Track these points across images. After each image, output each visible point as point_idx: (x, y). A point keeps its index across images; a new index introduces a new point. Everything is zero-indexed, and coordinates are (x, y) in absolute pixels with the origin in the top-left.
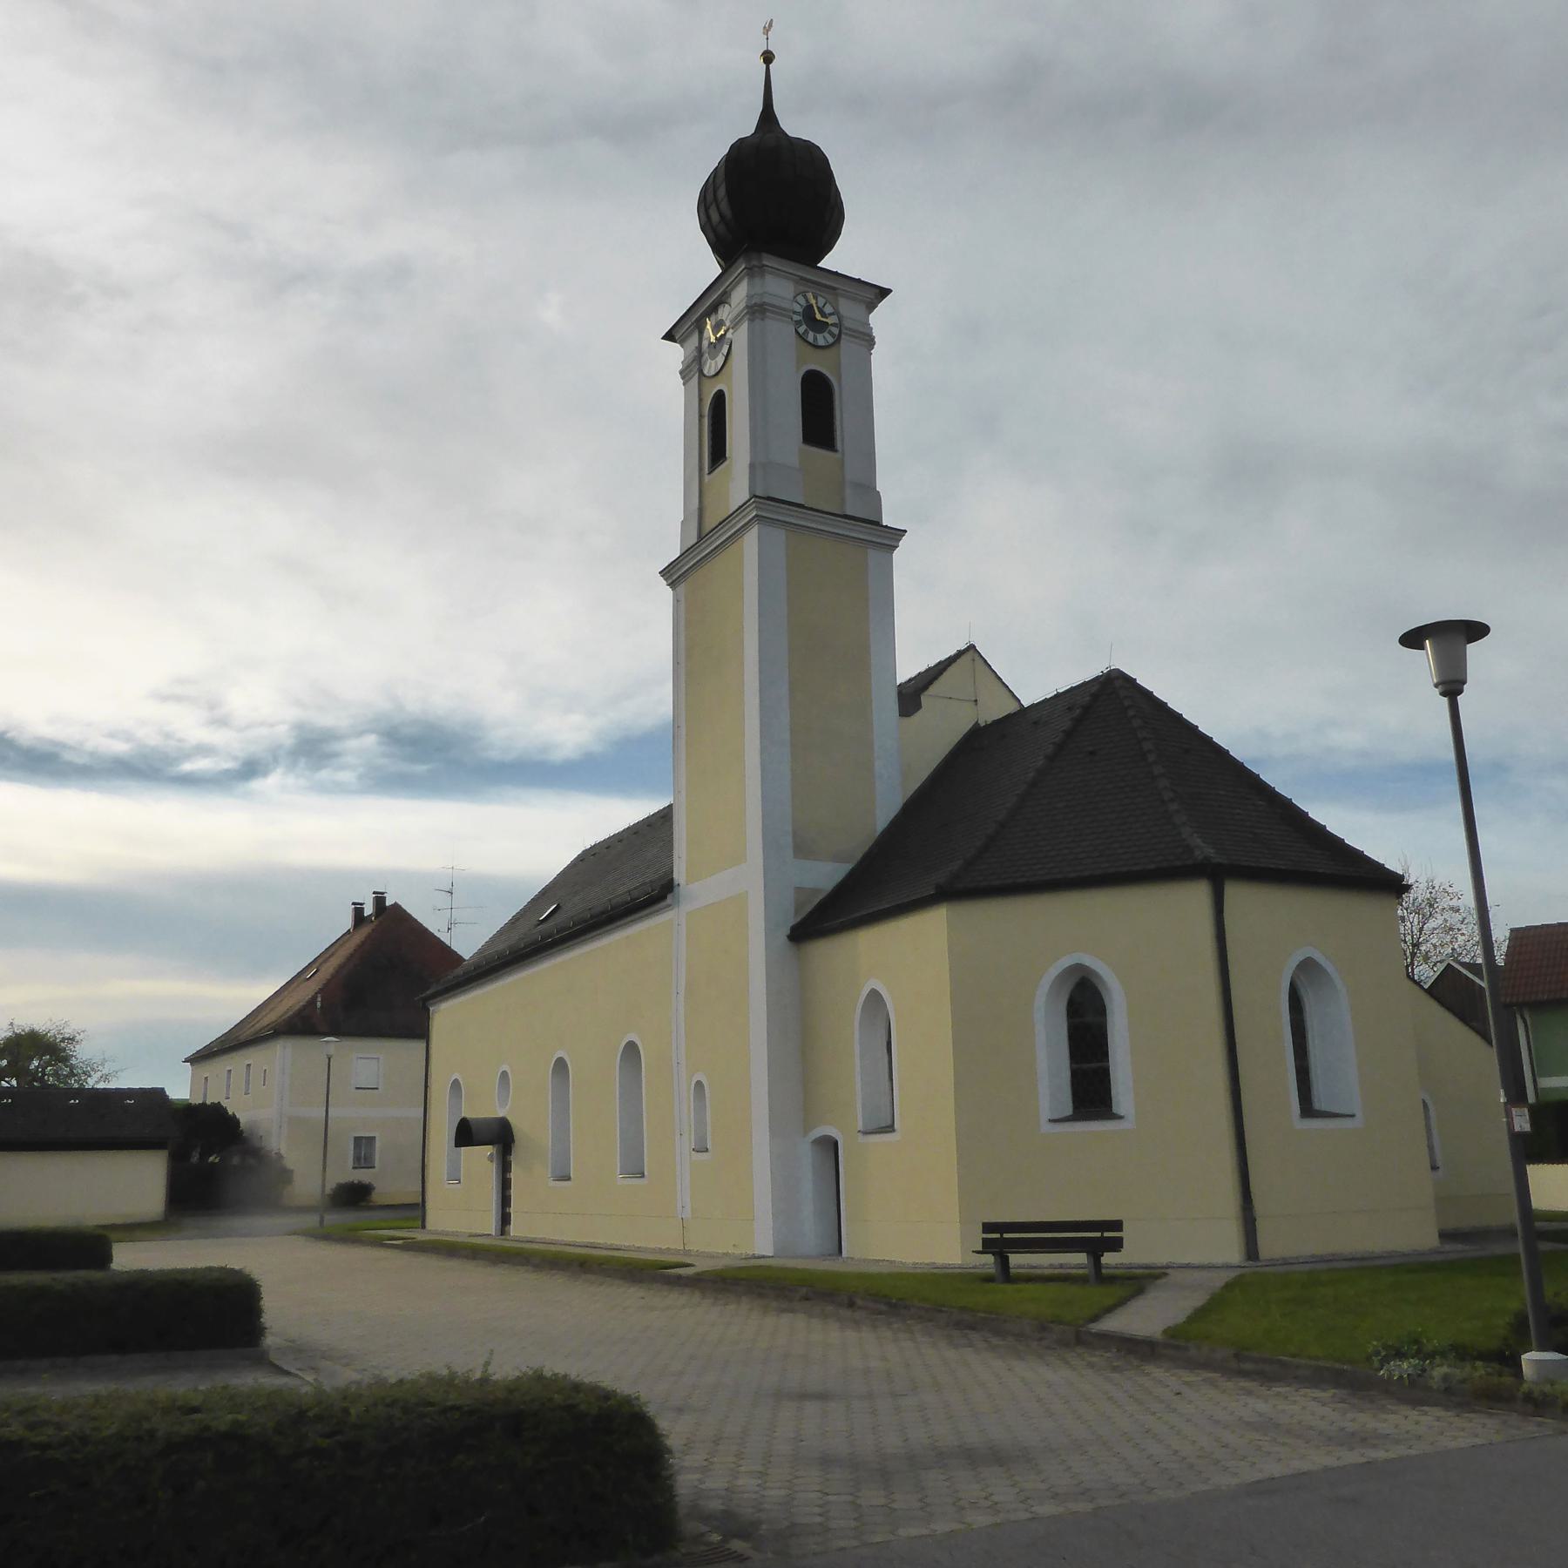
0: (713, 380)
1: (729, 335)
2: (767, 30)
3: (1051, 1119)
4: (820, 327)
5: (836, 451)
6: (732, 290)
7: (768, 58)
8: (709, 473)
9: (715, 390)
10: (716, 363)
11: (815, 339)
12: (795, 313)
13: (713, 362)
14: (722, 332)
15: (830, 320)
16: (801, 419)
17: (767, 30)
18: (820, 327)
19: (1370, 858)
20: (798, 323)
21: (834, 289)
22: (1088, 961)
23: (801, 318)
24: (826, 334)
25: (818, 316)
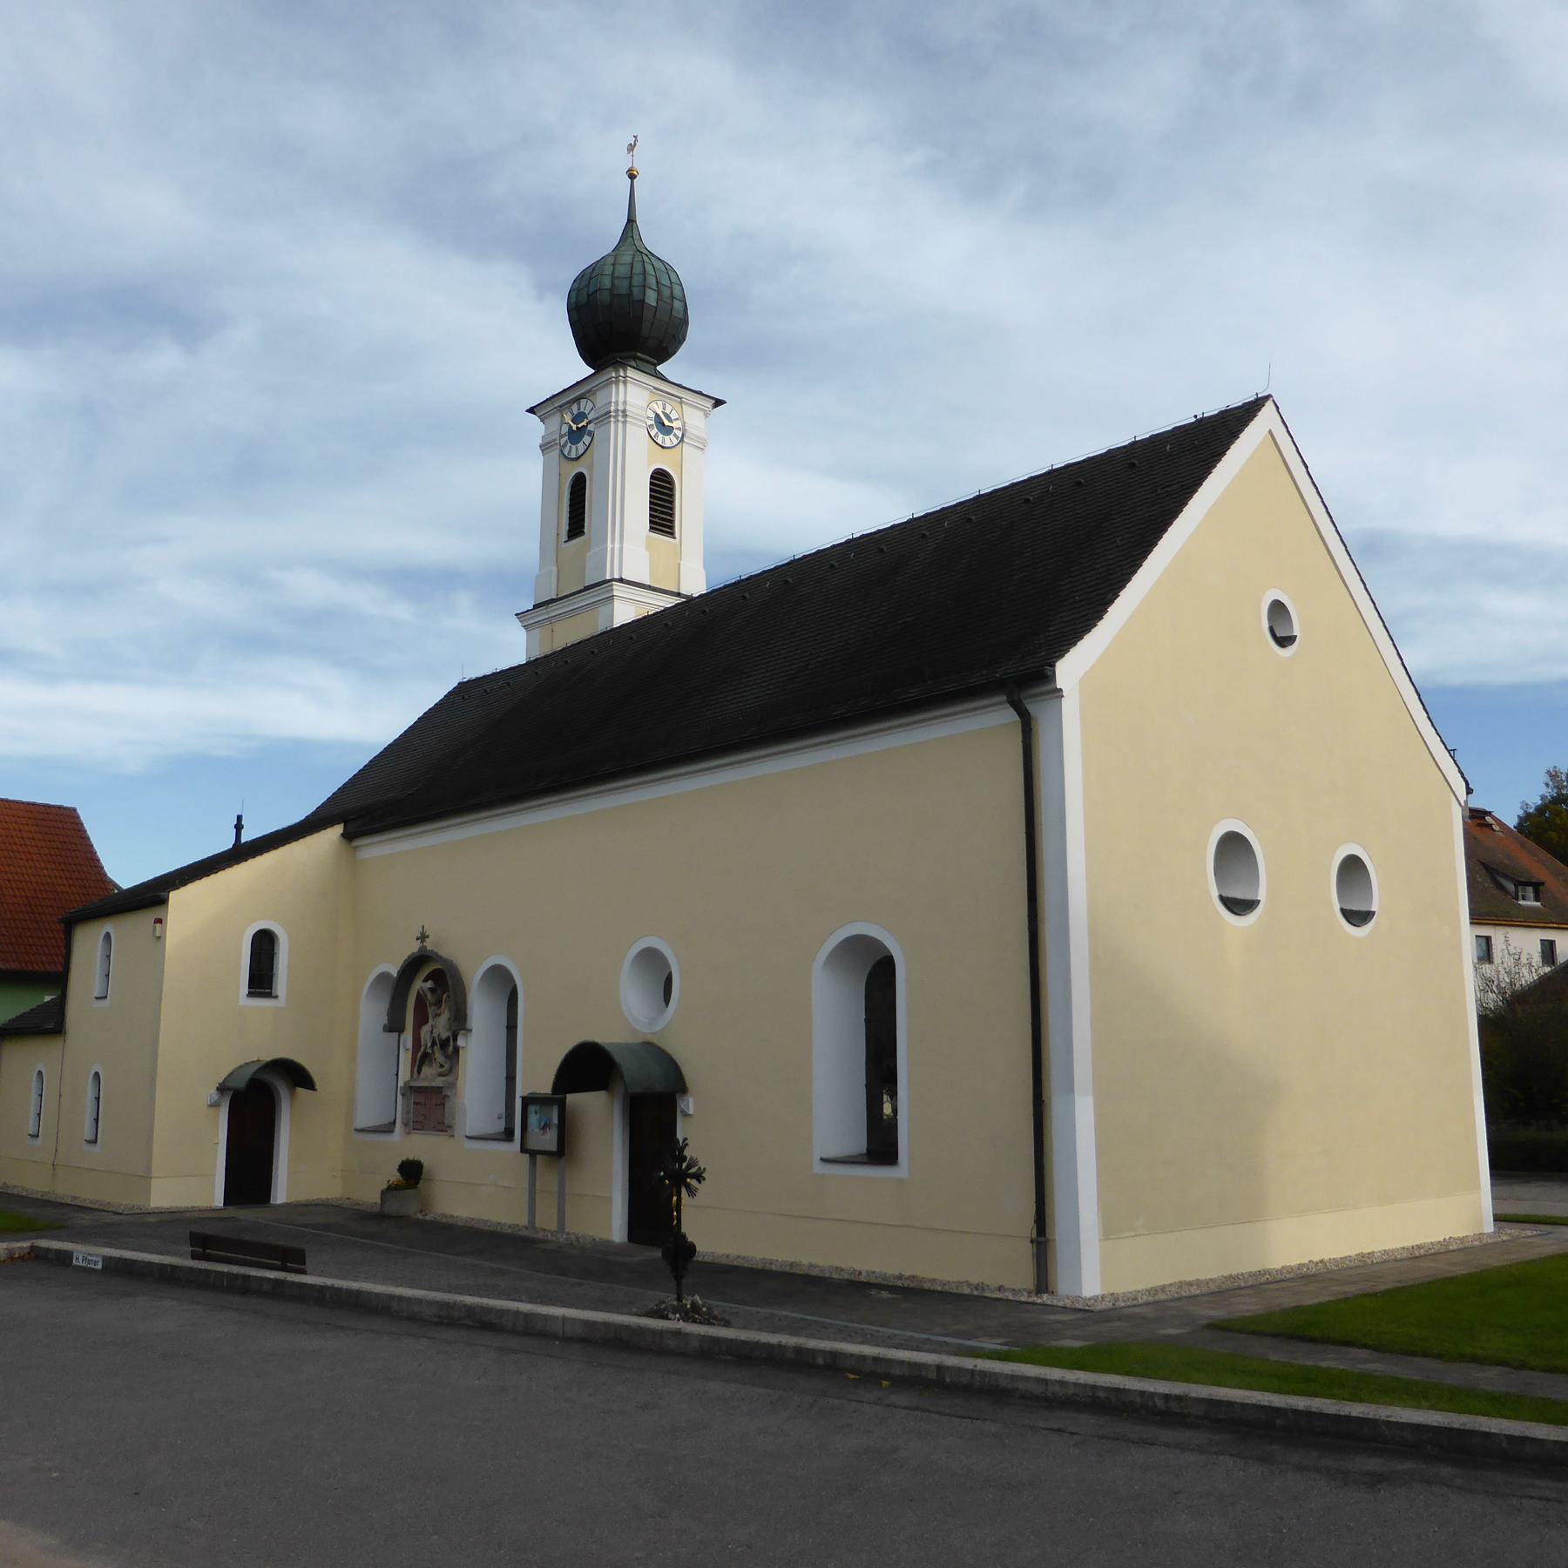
0: (574, 462)
1: (591, 427)
2: (631, 148)
3: (825, 1156)
4: (667, 430)
5: (675, 538)
6: (600, 389)
7: (632, 177)
8: (565, 542)
9: (577, 471)
10: (577, 449)
11: (656, 435)
12: (648, 418)
13: (574, 447)
14: (584, 423)
15: (674, 425)
16: (1069, 890)
17: (631, 148)
18: (667, 430)
19: (1479, 1024)
20: (651, 426)
21: (681, 398)
22: (1261, 906)
23: (653, 422)
24: (672, 436)
25: (667, 423)
